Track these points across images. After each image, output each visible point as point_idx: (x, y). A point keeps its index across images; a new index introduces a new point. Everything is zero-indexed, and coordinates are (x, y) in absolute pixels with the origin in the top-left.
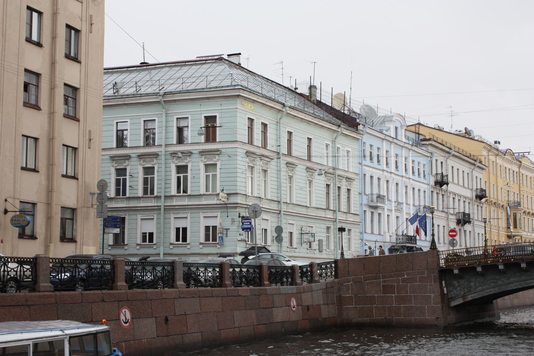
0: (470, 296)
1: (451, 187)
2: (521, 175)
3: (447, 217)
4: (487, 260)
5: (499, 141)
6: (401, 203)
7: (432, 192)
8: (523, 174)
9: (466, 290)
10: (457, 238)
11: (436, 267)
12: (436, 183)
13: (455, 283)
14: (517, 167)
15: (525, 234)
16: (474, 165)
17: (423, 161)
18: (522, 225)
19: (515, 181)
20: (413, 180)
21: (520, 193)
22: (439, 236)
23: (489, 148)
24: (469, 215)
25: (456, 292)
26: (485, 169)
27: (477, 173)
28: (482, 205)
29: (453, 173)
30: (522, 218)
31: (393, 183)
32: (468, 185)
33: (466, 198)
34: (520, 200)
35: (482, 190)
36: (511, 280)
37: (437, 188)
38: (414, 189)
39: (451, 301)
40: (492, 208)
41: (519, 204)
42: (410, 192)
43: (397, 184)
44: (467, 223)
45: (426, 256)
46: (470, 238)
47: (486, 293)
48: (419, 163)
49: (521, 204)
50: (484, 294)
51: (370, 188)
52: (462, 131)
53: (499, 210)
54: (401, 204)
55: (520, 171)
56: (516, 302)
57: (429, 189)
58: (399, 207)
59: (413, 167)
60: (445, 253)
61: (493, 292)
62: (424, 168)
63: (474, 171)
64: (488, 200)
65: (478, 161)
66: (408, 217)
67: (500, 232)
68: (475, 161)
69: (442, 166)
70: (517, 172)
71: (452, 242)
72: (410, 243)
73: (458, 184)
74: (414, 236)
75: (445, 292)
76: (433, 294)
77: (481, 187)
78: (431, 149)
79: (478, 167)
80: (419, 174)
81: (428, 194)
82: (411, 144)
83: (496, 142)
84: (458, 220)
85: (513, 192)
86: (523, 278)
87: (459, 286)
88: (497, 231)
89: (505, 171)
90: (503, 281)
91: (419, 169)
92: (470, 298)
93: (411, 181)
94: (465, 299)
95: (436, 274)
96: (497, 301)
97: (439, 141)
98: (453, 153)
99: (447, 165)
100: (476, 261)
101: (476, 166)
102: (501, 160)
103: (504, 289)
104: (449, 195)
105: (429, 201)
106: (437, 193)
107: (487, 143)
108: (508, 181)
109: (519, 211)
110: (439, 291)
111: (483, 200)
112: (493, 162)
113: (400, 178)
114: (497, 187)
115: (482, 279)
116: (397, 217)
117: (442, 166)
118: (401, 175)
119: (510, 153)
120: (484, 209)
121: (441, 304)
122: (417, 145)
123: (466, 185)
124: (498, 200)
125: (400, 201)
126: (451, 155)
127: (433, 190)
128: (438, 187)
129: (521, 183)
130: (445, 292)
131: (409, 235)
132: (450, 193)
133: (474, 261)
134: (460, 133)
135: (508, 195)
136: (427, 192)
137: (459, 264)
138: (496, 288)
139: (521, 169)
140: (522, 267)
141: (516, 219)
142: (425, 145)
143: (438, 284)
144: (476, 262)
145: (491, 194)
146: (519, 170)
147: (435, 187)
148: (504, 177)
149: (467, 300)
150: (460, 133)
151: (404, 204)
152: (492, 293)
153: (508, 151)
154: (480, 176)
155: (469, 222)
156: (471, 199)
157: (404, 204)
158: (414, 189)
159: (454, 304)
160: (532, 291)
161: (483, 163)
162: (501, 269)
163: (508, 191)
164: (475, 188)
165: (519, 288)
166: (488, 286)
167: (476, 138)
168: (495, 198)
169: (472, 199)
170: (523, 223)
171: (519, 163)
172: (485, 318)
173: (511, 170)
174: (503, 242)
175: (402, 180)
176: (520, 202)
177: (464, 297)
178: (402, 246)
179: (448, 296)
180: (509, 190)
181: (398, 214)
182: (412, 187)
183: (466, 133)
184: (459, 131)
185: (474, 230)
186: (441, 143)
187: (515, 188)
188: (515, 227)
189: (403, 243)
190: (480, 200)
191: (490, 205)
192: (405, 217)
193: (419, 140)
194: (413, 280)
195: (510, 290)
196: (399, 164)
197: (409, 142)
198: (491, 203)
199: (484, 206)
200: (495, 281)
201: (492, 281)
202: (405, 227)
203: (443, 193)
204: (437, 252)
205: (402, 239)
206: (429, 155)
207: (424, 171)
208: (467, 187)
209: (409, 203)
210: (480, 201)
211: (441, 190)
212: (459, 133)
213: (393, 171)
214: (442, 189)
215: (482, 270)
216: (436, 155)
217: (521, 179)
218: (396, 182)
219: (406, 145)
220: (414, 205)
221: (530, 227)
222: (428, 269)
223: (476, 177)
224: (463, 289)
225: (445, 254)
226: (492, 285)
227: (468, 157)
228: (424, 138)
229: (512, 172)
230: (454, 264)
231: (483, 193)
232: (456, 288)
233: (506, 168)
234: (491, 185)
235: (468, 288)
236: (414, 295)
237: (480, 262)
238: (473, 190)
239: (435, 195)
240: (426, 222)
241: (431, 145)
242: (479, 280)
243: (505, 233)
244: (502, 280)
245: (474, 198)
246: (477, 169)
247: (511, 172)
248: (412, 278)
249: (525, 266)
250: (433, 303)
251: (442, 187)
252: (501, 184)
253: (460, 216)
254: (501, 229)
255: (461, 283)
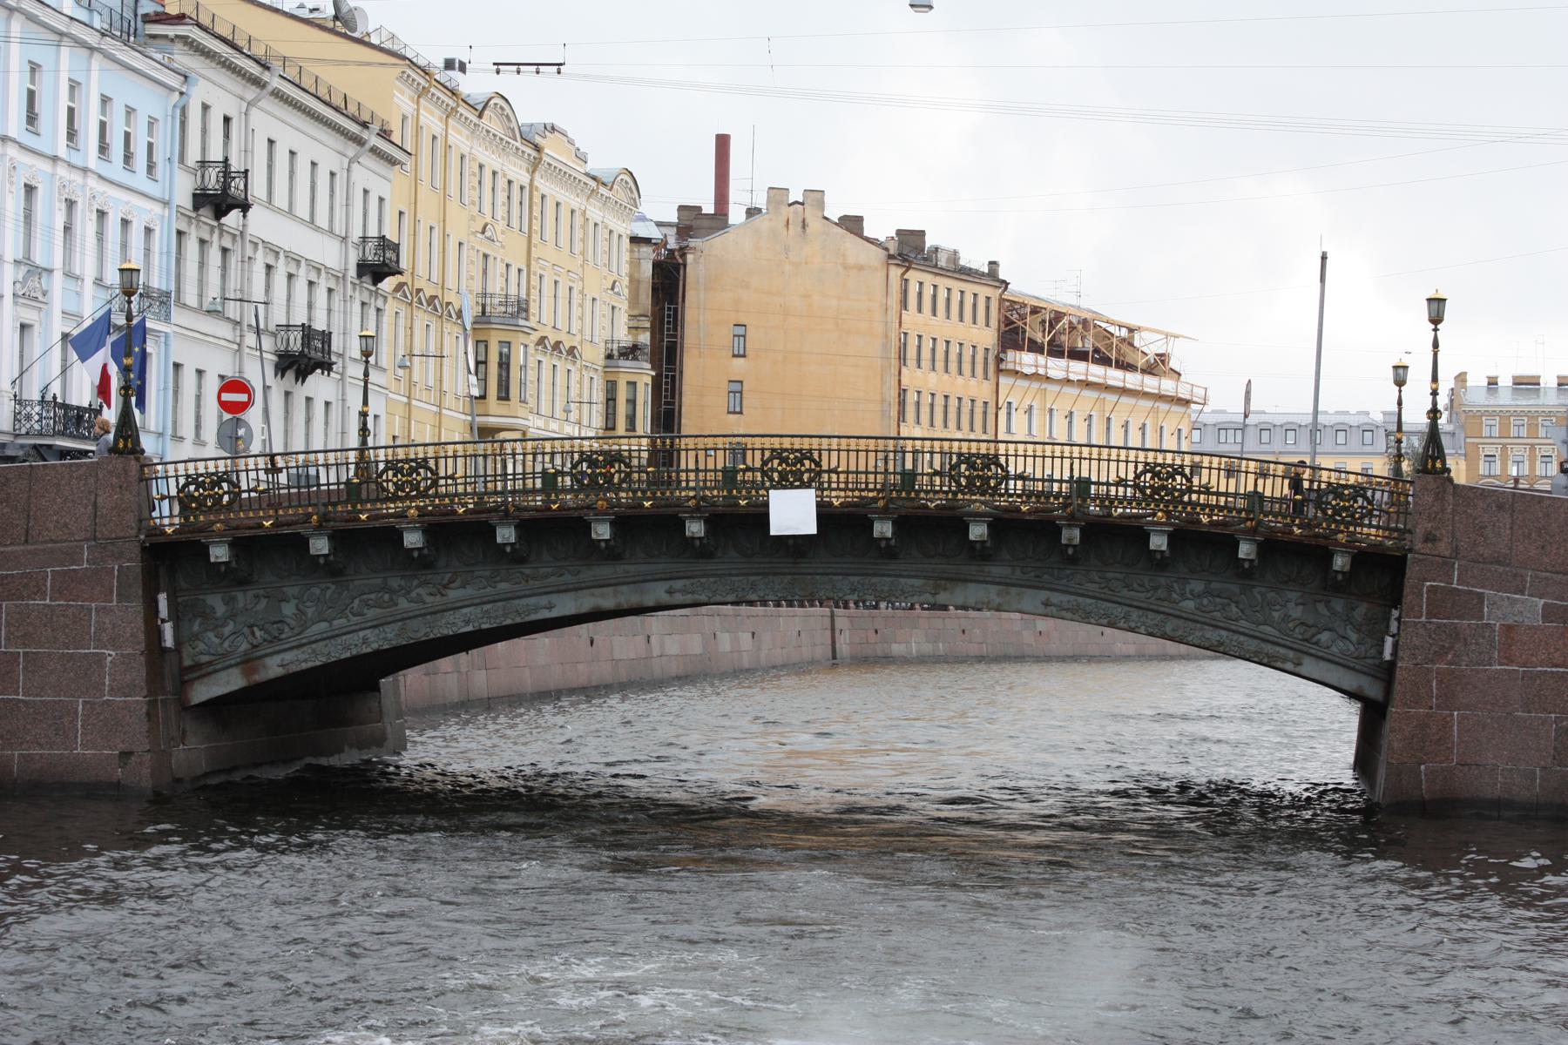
0: (277, 659)
1: (260, 222)
2: (537, 199)
3: (238, 340)
4: (354, 506)
5: (465, 60)
6: (45, 270)
7: (180, 233)
8: (543, 197)
9: (258, 633)
10: (253, 416)
11: (133, 532)
12: (363, 268)
13: (216, 603)
14: (525, 165)
15: (540, 423)
16: (359, 141)
17: (151, 103)
18: (531, 389)
19: (515, 223)
20: (100, 176)
21: (529, 266)
22: (202, 413)
23: (451, 102)
24: (326, 337)
25: (217, 641)
26: (402, 164)
27: (368, 174)
28: (380, 303)
29: (270, 167)
30: (532, 363)
31: (11, 183)
32: (331, 221)
33: (298, 262)
34: (528, 294)
35: (384, 243)
36: (453, 594)
37: (203, 219)
38: (101, 214)
39: (192, 681)
40: (422, 318)
41: (522, 308)
42: (86, 226)
43: (30, 189)
44: (319, 371)
45: (92, 480)
46: (326, 429)
47: (347, 648)
48: (130, 111)
49: (532, 310)
50: (337, 651)
51: (95, 260)
52: (322, 8)
53: (448, 327)
54: (44, 275)
55: (536, 183)
56: (481, 682)
57: (166, 220)
58: (33, 283)
59: (103, 125)
60: (176, 470)
61: (375, 646)
62: (150, 133)
63: (355, 166)
64: (405, 284)
65: (375, 127)
66: (67, 330)
67: (444, 411)
68: (365, 125)
69: (227, 135)
70: (522, 188)
71: (229, 433)
72: (72, 436)
73: (290, 212)
74: (90, 409)
75: (169, 641)
76: (115, 648)
77: (380, 231)
78: (184, 59)
79: (277, 94)
80: (128, 158)
81: (163, 240)
82: (97, 25)
83: (449, 64)
84: (280, 356)
85: (502, 260)
86: (503, 586)
87: (232, 616)
88: (435, 409)
89: (478, 179)
90: (420, 600)
91: (127, 135)
92: (273, 668)
93: (92, 182)
94: (254, 671)
95: (132, 562)
96: (396, 680)
97: (221, 30)
98: (276, 83)
99: (249, 132)
100: (310, 510)
101: (367, 147)
102: (466, 132)
103: (421, 631)
104: (249, 251)
105: (164, 266)
106: (202, 242)
107: (415, 60)
108: (488, 219)
109: (521, 335)
110: (142, 637)
111: (388, 284)
112: (434, 138)
113: (45, 166)
114: (445, 236)
115: (333, 587)
116: (23, 327)
117: (227, 135)
118: (49, 152)
119: (502, 108)
120: (387, 319)
121: (145, 692)
122: (125, 36)
123: (322, 220)
124: (443, 288)
125: (39, 259)
126: (265, 91)
127: (183, 227)
128: (206, 215)
129: (534, 227)
130: (169, 641)
131: (74, 402)
132: (256, 244)
133: (300, 511)
134: (315, 15)
135: (485, 272)
136: (157, 234)
137: (234, 524)
138: (387, 628)
139: (537, 175)
140: (499, 540)
141: (508, 365)
142: (158, 42)
143: (136, 607)
144: (310, 515)
145: (417, 262)
146: (532, 181)
147: (194, 215)
148: (473, 203)
149: (259, 677)
150: (315, 15)
151: (58, 276)
152: (369, 650)
153: (492, 102)
154: (379, 187)
155: (327, 367)
156: (341, 278)
157: (58, 276)
158: (101, 214)
159: (202, 692)
160: (547, 640)
161: (396, 138)
162: (413, 549)
163: (486, 256)
164: (356, 233)
165: (481, 631)
166: (354, 619)
167: (375, 40)
168: (434, 279)
169: (344, 277)
170: (532, 382)
171: (534, 154)
172: (340, 751)
173: (499, 175)
174: (394, 437)
175: (53, 175)
176: (527, 301)
177: (248, 663)
178: (35, 447)
179: (181, 659)
180: (487, 252)
181: (29, 316)
182: (96, 207)
183: (336, 18)
184: (312, 11)
185: (343, 400)
186: (230, 38)
187: (511, 249)
188: (504, 395)
189: (40, 434)
190: (375, 283)
191: (411, 304)
192: (58, 327)
193: (136, 15)
194: (25, 586)
195: (446, 638)
196: (42, 107)
197: (92, 19)
198: (412, 297)
199: (391, 307)
200: (386, 597)
201: (373, 596)
202: (57, 370)
203: (227, 243)
204: (143, 466)
205: (37, 418)
206: (174, 81)
207: (150, 145)
208: (325, 226)
209: (78, 272)
210: (373, 288)
211: (217, 231)
212: (312, 16)
213: (12, 133)
214: (221, 225)
215: (334, 549)
216: (202, 83)
217: (537, 213)
218: (23, 180)
219: (77, 30)
220: (99, 282)
221: (558, 398)
222: (95, 539)
223: (366, 192)
224: (246, 630)
225: (177, 477)
226: (371, 613)
227: (336, 109)
228: (160, 9)
229: (506, 187)
230: (214, 523)
231: (388, 255)
232: (217, 627)
233: (481, 166)
234: (423, 231)
235: (267, 626)
236: (25, 654)
237: (325, 518)
238: (350, 240)
239: (192, 247)
240: (144, 356)
241: (184, 39)
242: (316, 591)
243: (463, 417)
244: (414, 594)
245: (352, 272)
246: (368, 160)
247: (501, 183)
248: (22, 576)
249: (513, 540)
250: (112, 689)
251: (224, 220)
252: (460, 225)
253: (292, 338)
254: (449, 401)
255: (241, 605)
